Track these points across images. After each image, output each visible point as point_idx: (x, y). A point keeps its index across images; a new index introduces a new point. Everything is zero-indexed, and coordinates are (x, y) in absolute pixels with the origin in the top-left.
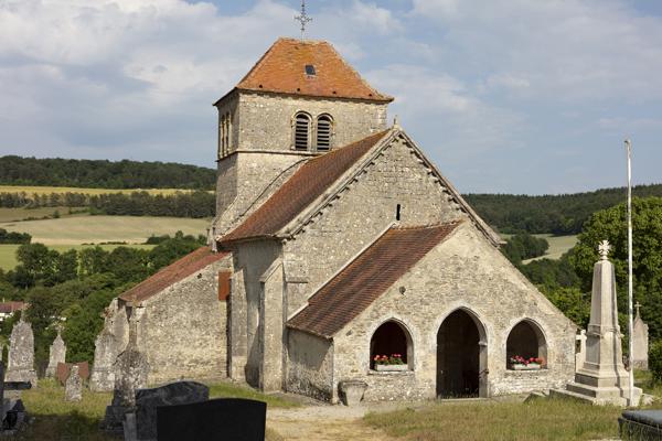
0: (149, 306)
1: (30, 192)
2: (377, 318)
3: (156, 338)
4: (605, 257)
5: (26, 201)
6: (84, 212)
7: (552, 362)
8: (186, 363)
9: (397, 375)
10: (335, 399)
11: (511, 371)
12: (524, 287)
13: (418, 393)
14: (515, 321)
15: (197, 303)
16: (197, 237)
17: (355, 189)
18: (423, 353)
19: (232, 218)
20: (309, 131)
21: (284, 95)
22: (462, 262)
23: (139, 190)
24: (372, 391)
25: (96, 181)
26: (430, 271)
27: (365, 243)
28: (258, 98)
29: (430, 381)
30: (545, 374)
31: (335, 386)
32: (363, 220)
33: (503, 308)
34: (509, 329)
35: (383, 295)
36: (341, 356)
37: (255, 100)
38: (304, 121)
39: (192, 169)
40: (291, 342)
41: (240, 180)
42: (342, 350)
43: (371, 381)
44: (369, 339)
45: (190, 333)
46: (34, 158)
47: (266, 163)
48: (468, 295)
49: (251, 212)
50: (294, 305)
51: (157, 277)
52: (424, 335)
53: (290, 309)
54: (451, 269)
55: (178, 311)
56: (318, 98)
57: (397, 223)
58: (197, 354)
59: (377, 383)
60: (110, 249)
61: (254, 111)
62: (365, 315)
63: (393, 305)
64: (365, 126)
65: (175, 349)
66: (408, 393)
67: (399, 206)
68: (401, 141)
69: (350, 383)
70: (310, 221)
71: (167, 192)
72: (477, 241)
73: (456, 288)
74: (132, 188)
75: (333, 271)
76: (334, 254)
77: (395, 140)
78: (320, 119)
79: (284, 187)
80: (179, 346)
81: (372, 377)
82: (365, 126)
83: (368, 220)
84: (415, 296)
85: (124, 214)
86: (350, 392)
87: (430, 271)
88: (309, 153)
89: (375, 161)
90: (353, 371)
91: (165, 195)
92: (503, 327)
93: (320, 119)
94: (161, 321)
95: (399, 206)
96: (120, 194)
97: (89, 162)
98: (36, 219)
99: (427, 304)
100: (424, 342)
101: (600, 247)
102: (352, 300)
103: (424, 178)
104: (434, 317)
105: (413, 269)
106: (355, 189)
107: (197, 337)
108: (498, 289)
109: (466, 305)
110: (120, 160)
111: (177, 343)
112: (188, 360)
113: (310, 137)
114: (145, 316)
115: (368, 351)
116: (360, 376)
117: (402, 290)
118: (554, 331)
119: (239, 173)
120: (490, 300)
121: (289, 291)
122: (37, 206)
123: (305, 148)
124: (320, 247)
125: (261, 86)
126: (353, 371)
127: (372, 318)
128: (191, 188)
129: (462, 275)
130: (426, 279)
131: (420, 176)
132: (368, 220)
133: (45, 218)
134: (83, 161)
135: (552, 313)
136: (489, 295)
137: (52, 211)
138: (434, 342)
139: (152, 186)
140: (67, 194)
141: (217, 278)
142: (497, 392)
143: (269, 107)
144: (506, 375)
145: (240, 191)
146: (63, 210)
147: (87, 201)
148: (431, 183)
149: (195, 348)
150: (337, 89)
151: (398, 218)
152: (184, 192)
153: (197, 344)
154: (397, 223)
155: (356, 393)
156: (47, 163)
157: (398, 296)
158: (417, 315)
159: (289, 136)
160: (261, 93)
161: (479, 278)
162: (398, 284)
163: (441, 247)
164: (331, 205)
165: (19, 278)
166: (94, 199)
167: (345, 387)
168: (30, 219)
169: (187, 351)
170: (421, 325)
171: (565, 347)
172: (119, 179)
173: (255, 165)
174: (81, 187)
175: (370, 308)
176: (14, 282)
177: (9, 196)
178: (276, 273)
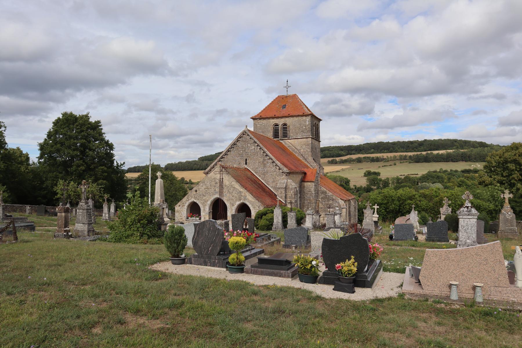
1: (385, 155)
2: (188, 201)
4: (159, 176)
5: (384, 159)
6: (406, 162)
12: (241, 190)
14: (238, 203)
16: (438, 170)
18: (204, 214)
21: (269, 118)
22: (217, 181)
23: (429, 152)
26: (206, 184)
28: (259, 121)
37: (259, 121)
38: (278, 127)
39: (455, 141)
42: (178, 212)
46: (389, 142)
60: (403, 177)
61: (258, 126)
64: (302, 126)
67: (246, 159)
71: (441, 152)
73: (215, 190)
78: (283, 126)
81: (187, 221)
82: (302, 126)
85: (422, 162)
87: (206, 184)
90: (181, 219)
91: (440, 153)
92: (233, 205)
93: (283, 126)
95: (246, 159)
96: (421, 154)
98: (387, 166)
100: (204, 210)
101: (157, 174)
106: (230, 154)
110: (423, 140)
117: (196, 191)
118: (254, 208)
122: (388, 161)
123: (278, 138)
125: (261, 116)
128: (454, 149)
130: (204, 187)
131: (254, 147)
133: (391, 165)
135: (253, 200)
140: (400, 156)
143: (264, 123)
146: (398, 163)
147: (408, 158)
148: (259, 150)
151: (246, 164)
152: (449, 151)
156: (394, 144)
157: (195, 193)
160: (260, 119)
164: (221, 161)
165: (367, 189)
166: (410, 156)
168: (385, 166)
174: (407, 152)
176: (366, 191)
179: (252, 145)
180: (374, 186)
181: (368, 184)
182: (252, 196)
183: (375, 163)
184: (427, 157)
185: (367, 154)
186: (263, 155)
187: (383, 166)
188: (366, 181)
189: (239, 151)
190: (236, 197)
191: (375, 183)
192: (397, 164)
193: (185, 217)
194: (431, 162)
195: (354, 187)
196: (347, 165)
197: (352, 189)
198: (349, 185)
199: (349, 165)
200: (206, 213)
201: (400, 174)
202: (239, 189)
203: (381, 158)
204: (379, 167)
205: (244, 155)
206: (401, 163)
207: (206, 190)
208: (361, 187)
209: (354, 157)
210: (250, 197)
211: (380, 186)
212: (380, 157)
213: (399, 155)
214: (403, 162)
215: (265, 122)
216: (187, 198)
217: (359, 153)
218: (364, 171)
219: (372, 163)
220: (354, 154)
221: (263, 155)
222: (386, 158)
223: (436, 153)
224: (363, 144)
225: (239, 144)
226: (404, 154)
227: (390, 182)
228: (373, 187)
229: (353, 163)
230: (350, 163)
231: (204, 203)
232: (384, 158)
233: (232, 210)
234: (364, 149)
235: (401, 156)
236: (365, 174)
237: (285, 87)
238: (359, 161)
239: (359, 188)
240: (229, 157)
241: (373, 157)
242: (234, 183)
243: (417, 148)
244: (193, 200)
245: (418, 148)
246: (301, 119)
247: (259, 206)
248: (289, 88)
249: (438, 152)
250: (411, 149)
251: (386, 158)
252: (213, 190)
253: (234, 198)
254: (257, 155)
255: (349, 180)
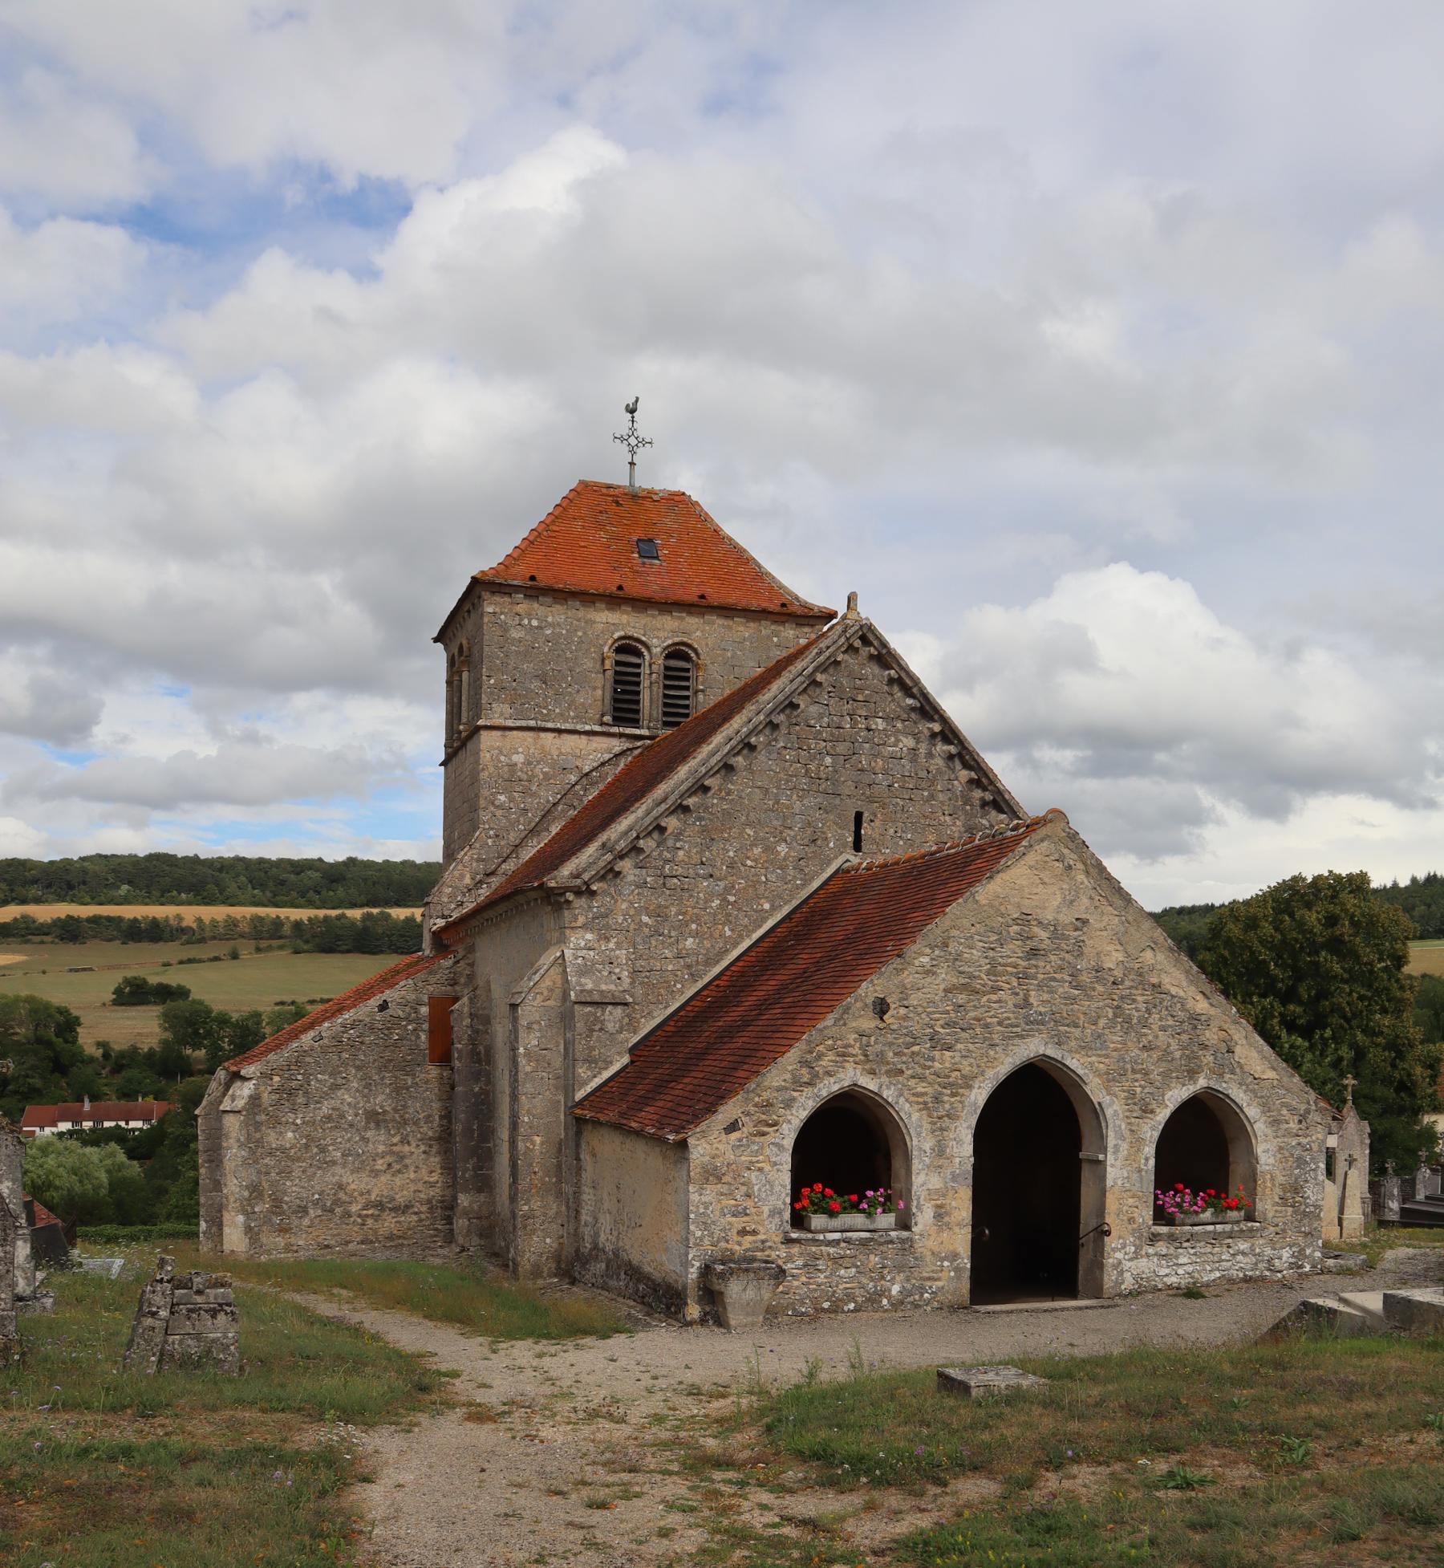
0: (266, 1076)
1: (190, 914)
2: (809, 1084)
3: (283, 1150)
5: (183, 931)
6: (281, 948)
7: (1267, 1204)
8: (354, 1208)
9: (864, 1243)
10: (693, 1311)
11: (1164, 1230)
12: (1202, 1006)
13: (922, 1290)
14: (1177, 1095)
15: (380, 1070)
17: (749, 768)
18: (935, 1182)
19: (467, 880)
20: (645, 683)
21: (587, 598)
22: (1044, 935)
24: (796, 1284)
25: (303, 894)
26: (958, 957)
27: (774, 908)
29: (955, 1256)
30: (1250, 1234)
31: (693, 1273)
32: (766, 849)
33: (1149, 1060)
34: (1163, 1115)
35: (829, 1020)
36: (710, 1193)
37: (520, 608)
40: (585, 1156)
41: (485, 792)
42: (712, 1174)
43: (793, 1260)
44: (789, 1142)
45: (364, 1139)
47: (545, 752)
48: (1057, 1024)
49: (510, 866)
50: (590, 1061)
51: (503, 1084)
52: (940, 1128)
53: (582, 1071)
54: (1013, 952)
55: (335, 1087)
56: (668, 606)
57: (855, 859)
58: (379, 1187)
59: (810, 1266)
61: (515, 634)
62: (777, 1076)
63: (856, 1050)
65: (328, 1178)
66: (895, 1289)
67: (859, 817)
68: (866, 651)
69: (745, 1265)
70: (635, 849)
72: (1081, 877)
73: (1027, 1003)
74: (362, 906)
75: (694, 977)
76: (696, 935)
77: (851, 649)
79: (585, 808)
80: (338, 1170)
83: (782, 849)
84: (915, 1026)
85: (348, 951)
86: (737, 1291)
87: (958, 957)
88: (644, 732)
89: (802, 701)
90: (743, 1232)
92: (1147, 1111)
94: (294, 1110)
95: (859, 817)
96: (343, 916)
97: (290, 862)
98: (200, 961)
99: (949, 1049)
100: (940, 1151)
102: (739, 1042)
103: (923, 749)
104: (967, 1082)
105: (911, 949)
106: (749, 768)
107: (381, 1148)
108: (1133, 1011)
109: (1052, 1052)
111: (334, 1163)
112: (362, 1200)
113: (645, 697)
114: (255, 1099)
115: (786, 1178)
116: (763, 1245)
117: (881, 1008)
118: (1275, 1122)
119: (484, 775)
120: (1115, 1039)
121: (580, 1026)
122: (202, 940)
123: (635, 723)
124: (659, 914)
125: (533, 578)
126: (743, 1232)
127: (798, 1084)
129: (1043, 967)
130: (945, 976)
131: (909, 742)
132: (782, 849)
133: (216, 959)
134: (281, 861)
135: (1271, 1074)
136: (1111, 1025)
137: (221, 949)
138: (963, 1148)
139: (398, 904)
141: (424, 1010)
142: (1128, 1284)
143: (552, 625)
144: (1154, 1238)
145: (484, 816)
146: (246, 949)
147: (287, 929)
148: (940, 762)
149: (375, 1174)
150: (708, 591)
151: (857, 846)
153: (380, 1164)
154: (855, 859)
155: (750, 1294)
157: (869, 1023)
158: (922, 1078)
159: (596, 693)
161: (1085, 978)
162: (870, 989)
163: (987, 892)
166: (298, 925)
167: (722, 1275)
168: (190, 961)
169: (356, 1182)
170: (930, 1106)
171: (1300, 1162)
172: (341, 892)
173: (518, 759)
174: (277, 905)
175: (790, 1059)
177: (155, 922)
178: (548, 982)
179: (899, 725)
180: (196, 1046)
181: (169, 1035)
182: (1267, 1048)
183: (145, 946)
184: (365, 929)
185: (101, 904)
186: (967, 801)
187: (181, 962)
188: (160, 1025)
189: (812, 758)
190: (1167, 1052)
191: (196, 1033)
192: (244, 953)
193: (775, 1212)
194: (382, 952)
195: (101, 1051)
196: (13, 952)
197: (92, 1059)
198: (74, 1041)
199: (19, 952)
200: (954, 1178)
201: (278, 1000)
202: (1190, 1004)
203: (169, 926)
204: (165, 965)
205: (847, 788)
206: (258, 950)
207: (961, 998)
208: (134, 1049)
209: (46, 912)
210: (1255, 1054)
211: (221, 1049)
212: (167, 919)
213: (248, 916)
214: (270, 948)
215: (561, 619)
216: (804, 1063)
217: (61, 899)
218: (115, 979)
219: (132, 945)
220: (38, 901)
221: (967, 801)
222: (194, 926)
223: (402, 917)
224: (83, 859)
225: (813, 709)
226: (272, 912)
227: (267, 1030)
228: (189, 1052)
229: (42, 942)
230: (27, 942)
231: (937, 1099)
232: (184, 924)
233: (1138, 1143)
234: (84, 883)
235: (257, 920)
236: (118, 991)
237: (622, 439)
238: (69, 932)
239: (122, 1055)
240: (738, 785)
241: (135, 920)
242: (1161, 957)
243: (319, 893)
244: (851, 1076)
245: (324, 892)
246: (769, 638)
247: (1308, 1111)
248: (640, 451)
249: (408, 915)
250: (294, 894)
251: (191, 928)
252: (1011, 1002)
253: (1149, 1060)
254: (932, 797)
255: (77, 1018)
